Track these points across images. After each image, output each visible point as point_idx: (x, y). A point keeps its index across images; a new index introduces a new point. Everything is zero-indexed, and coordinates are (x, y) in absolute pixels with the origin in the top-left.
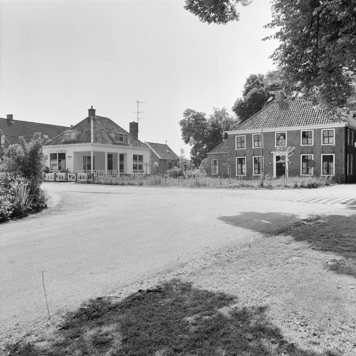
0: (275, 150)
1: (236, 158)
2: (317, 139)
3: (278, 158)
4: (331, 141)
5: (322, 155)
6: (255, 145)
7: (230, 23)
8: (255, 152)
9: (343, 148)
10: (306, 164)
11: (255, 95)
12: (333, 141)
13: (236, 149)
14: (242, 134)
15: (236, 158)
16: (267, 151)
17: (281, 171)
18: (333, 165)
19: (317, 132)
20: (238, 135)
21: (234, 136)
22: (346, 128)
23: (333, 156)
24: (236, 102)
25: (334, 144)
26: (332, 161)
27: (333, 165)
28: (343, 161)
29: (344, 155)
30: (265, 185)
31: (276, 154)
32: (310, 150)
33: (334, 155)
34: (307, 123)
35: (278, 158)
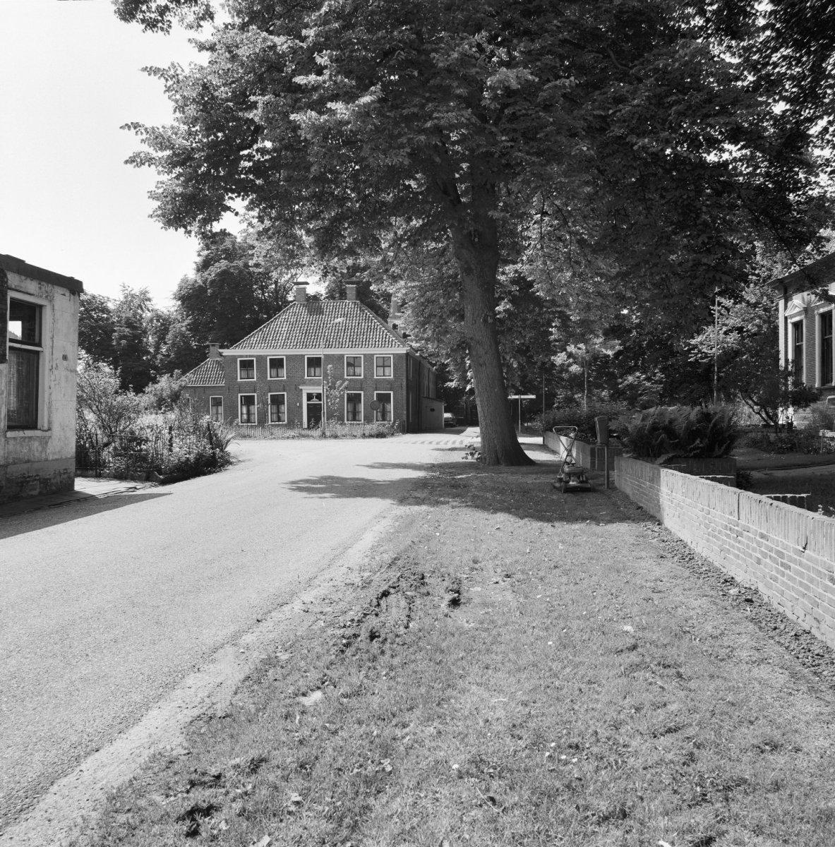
0: (304, 383)
1: (239, 395)
2: (369, 369)
3: (310, 397)
4: (387, 373)
5: (269, 394)
6: (378, 374)
7: (136, 26)
8: (378, 384)
9: (404, 383)
10: (352, 405)
11: (224, 274)
12: (390, 373)
13: (239, 380)
14: (250, 356)
15: (239, 395)
16: (293, 386)
17: (314, 413)
18: (391, 407)
19: (369, 358)
20: (241, 356)
21: (234, 358)
22: (407, 354)
23: (360, 394)
24: (181, 289)
25: (392, 377)
26: (253, 404)
27: (391, 407)
28: (405, 402)
29: (405, 393)
30: (328, 434)
31: (306, 390)
32: (252, 388)
33: (392, 393)
34: (353, 345)
35: (310, 397)
